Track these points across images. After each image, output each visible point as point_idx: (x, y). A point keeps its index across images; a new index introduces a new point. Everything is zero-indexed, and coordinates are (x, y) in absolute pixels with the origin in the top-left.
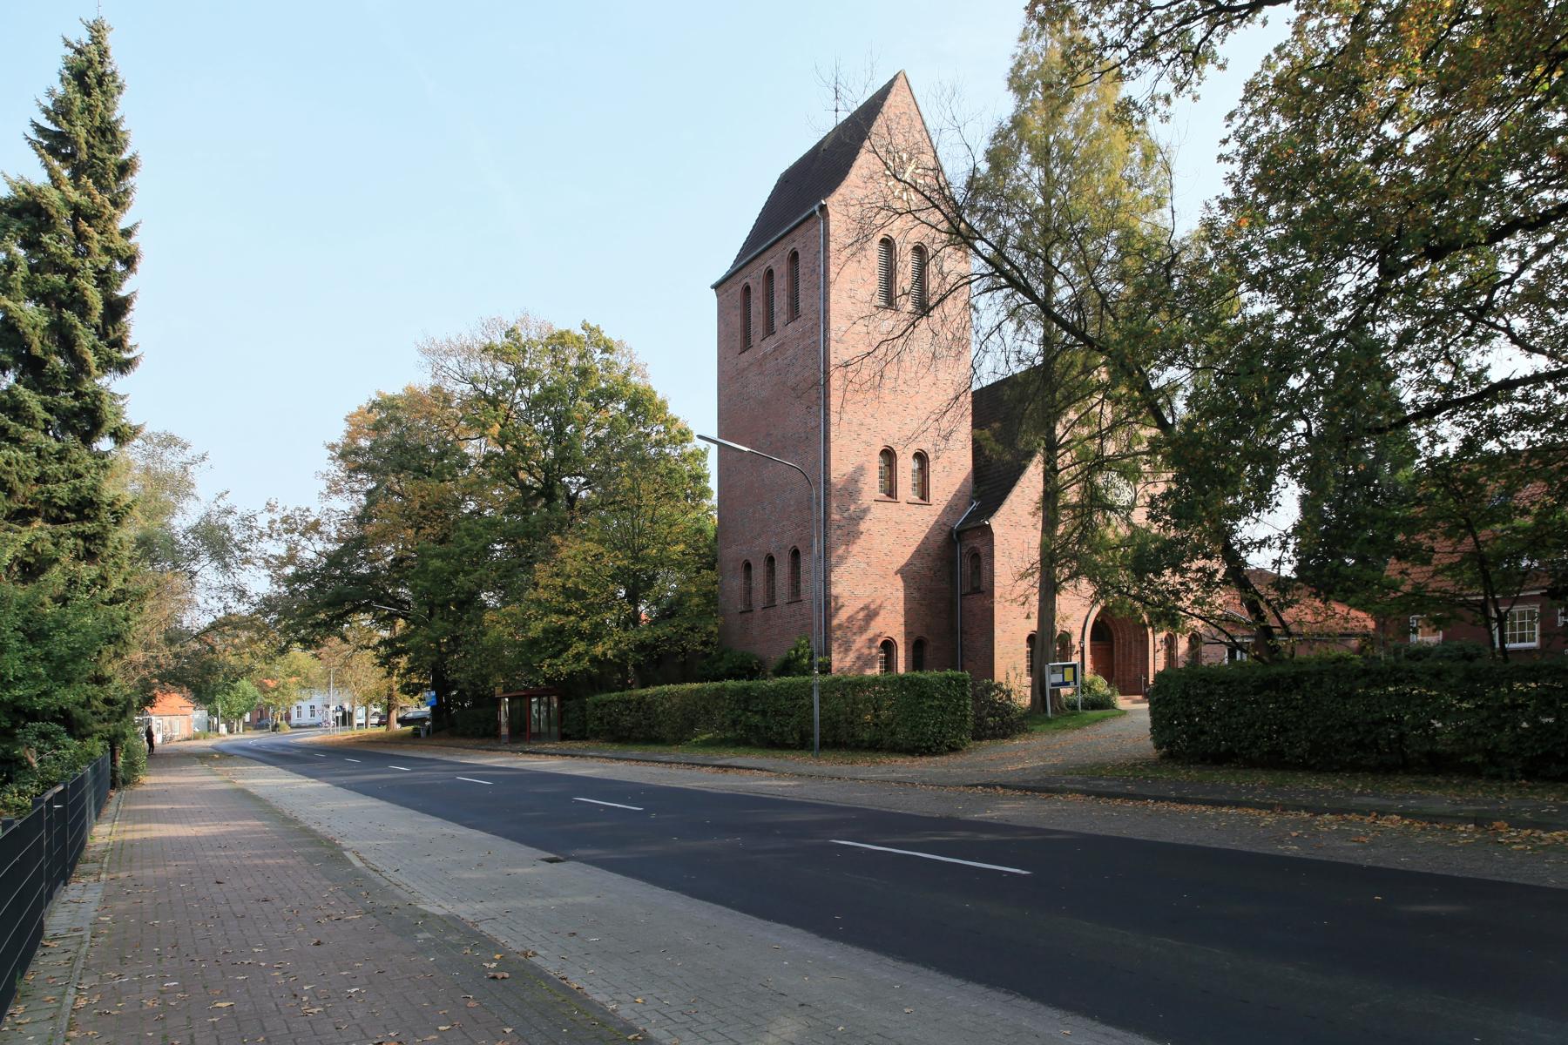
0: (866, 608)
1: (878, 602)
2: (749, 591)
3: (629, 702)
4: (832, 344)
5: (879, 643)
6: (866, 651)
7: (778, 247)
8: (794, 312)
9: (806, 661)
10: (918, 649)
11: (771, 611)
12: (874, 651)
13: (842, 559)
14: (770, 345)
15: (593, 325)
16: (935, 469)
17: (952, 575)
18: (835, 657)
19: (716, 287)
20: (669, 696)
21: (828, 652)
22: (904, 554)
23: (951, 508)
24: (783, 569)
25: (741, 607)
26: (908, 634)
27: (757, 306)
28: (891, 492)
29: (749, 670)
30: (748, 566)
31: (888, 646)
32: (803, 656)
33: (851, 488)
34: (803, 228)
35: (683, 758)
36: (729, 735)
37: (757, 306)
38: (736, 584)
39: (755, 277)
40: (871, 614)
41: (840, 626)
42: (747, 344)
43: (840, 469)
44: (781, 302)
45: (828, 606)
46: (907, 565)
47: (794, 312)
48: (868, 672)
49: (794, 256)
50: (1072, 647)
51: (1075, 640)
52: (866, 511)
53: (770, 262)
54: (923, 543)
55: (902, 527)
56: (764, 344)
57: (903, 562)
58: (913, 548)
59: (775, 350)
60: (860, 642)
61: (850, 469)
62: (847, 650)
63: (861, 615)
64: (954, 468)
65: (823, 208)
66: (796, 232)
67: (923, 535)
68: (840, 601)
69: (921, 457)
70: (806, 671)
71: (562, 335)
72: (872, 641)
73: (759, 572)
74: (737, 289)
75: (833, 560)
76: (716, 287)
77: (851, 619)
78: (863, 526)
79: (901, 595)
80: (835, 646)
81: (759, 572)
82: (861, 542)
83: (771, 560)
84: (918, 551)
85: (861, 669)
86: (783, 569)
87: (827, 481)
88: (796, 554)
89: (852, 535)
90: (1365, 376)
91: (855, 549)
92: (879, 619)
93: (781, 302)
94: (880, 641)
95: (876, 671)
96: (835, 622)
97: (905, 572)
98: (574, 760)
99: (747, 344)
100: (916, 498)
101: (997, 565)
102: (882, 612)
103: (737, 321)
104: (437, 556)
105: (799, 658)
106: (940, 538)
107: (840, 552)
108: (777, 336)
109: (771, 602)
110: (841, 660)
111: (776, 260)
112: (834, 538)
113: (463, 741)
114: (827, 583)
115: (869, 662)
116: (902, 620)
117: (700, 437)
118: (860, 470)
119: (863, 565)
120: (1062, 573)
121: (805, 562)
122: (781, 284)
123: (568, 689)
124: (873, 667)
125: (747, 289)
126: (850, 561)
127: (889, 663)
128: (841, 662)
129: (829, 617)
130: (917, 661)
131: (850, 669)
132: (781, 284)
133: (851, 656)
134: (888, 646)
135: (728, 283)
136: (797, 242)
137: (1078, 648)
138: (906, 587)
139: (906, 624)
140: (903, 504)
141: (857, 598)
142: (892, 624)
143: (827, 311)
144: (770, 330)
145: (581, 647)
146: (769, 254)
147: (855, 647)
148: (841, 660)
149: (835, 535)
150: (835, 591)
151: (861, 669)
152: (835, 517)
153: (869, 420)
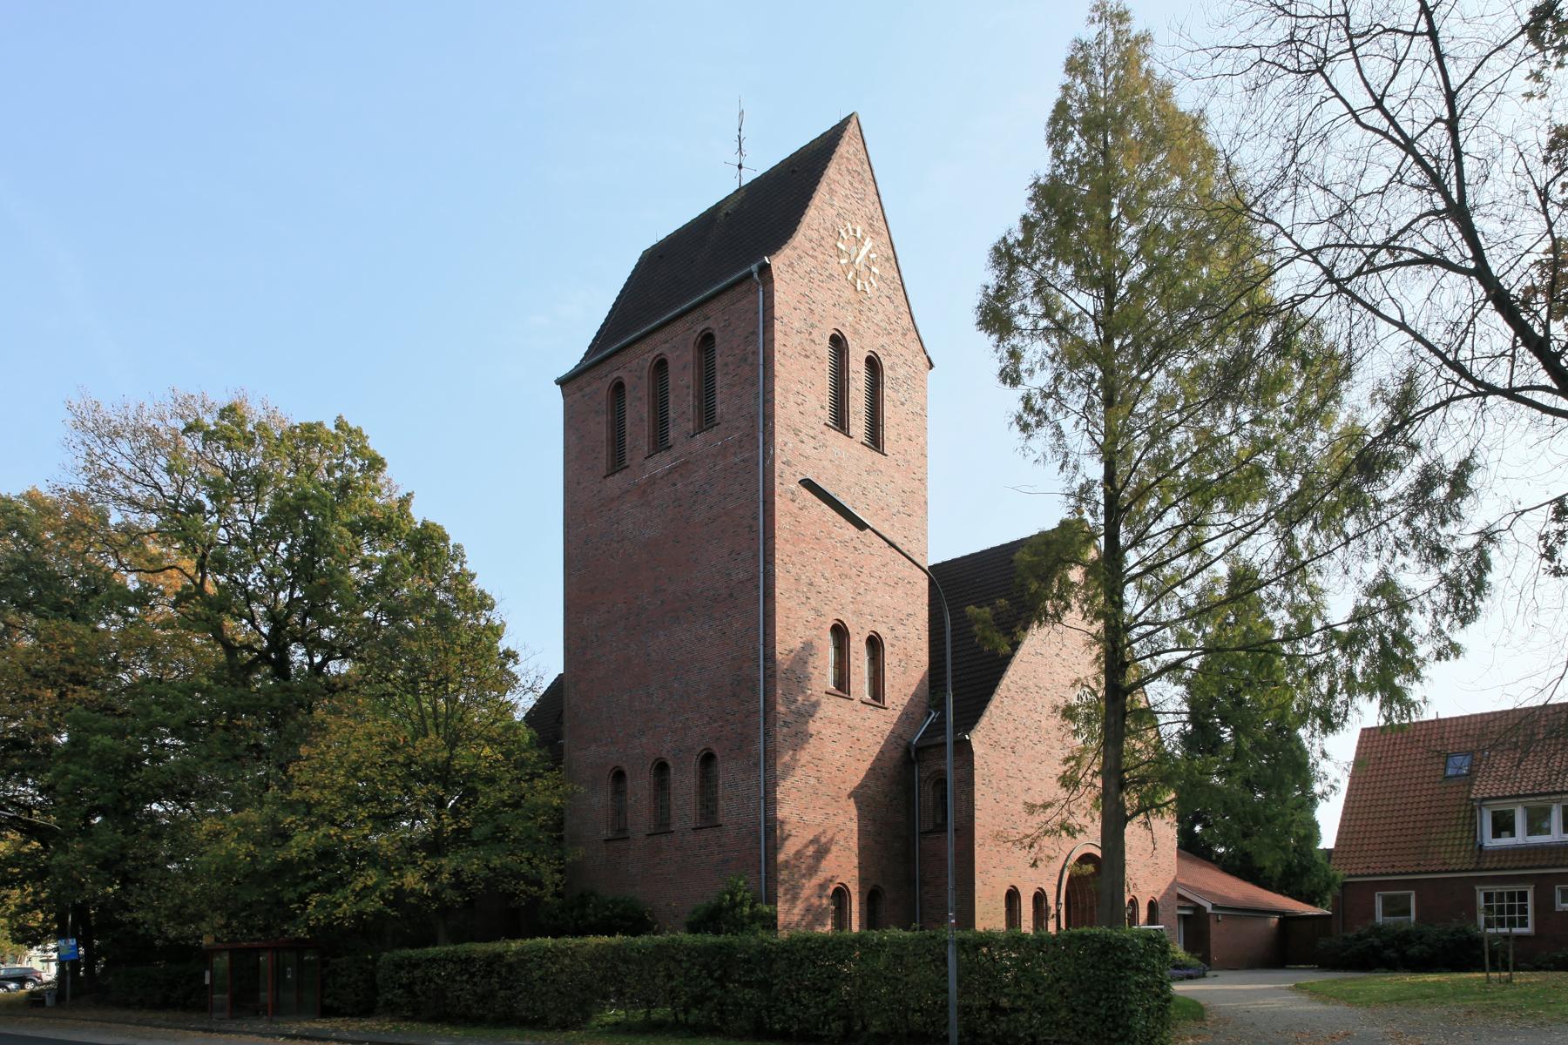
0: (815, 840)
1: (829, 835)
4: (778, 464)
5: (830, 891)
6: (815, 901)
7: (679, 326)
8: (706, 417)
9: (747, 910)
10: (872, 898)
12: (825, 902)
13: (789, 769)
14: (662, 463)
15: (353, 425)
16: (890, 658)
17: (910, 803)
18: (781, 907)
19: (563, 382)
20: (555, 955)
21: (772, 899)
22: (857, 772)
23: (907, 717)
24: (685, 782)
25: (606, 833)
26: (863, 881)
27: (638, 410)
28: (842, 683)
30: (619, 776)
31: (840, 895)
32: (742, 903)
34: (725, 299)
36: (658, 1014)
37: (638, 410)
38: (602, 798)
39: (634, 369)
40: (822, 852)
41: (787, 864)
42: (618, 462)
43: (787, 640)
44: (682, 403)
45: (771, 832)
46: (861, 786)
47: (706, 417)
48: (819, 930)
49: (707, 340)
50: (1048, 909)
51: (1051, 901)
52: (816, 705)
53: (663, 349)
55: (856, 734)
56: (650, 463)
58: (867, 765)
59: (671, 471)
60: (809, 887)
62: (795, 898)
63: (810, 850)
64: (909, 664)
65: (765, 269)
67: (877, 749)
70: (739, 926)
71: (309, 428)
72: (823, 887)
73: (640, 786)
74: (600, 387)
75: (779, 769)
76: (563, 382)
77: (799, 855)
78: (813, 727)
79: (854, 826)
80: (781, 891)
81: (640, 786)
82: (811, 748)
83: (662, 767)
85: (810, 925)
86: (685, 782)
87: (770, 657)
88: (708, 759)
91: (804, 756)
92: (831, 857)
93: (682, 403)
94: (832, 887)
95: (827, 928)
96: (781, 857)
97: (858, 795)
99: (618, 462)
100: (867, 697)
101: (977, 795)
102: (834, 848)
103: (600, 428)
104: (104, 731)
105: (735, 905)
106: (897, 754)
107: (787, 758)
109: (662, 826)
111: (678, 346)
113: (151, 1015)
114: (770, 802)
115: (819, 918)
116: (856, 861)
117: (808, 484)
118: (808, 647)
119: (813, 781)
120: (1131, 800)
121: (726, 771)
122: (682, 381)
123: (330, 941)
124: (823, 925)
126: (799, 772)
128: (789, 915)
130: (872, 918)
131: (798, 925)
132: (682, 381)
133: (799, 909)
134: (840, 895)
137: (1053, 911)
138: (861, 817)
139: (861, 867)
142: (844, 866)
143: (769, 417)
144: (660, 442)
145: (372, 877)
146: (660, 336)
147: (805, 893)
149: (782, 733)
150: (781, 813)
152: (781, 709)
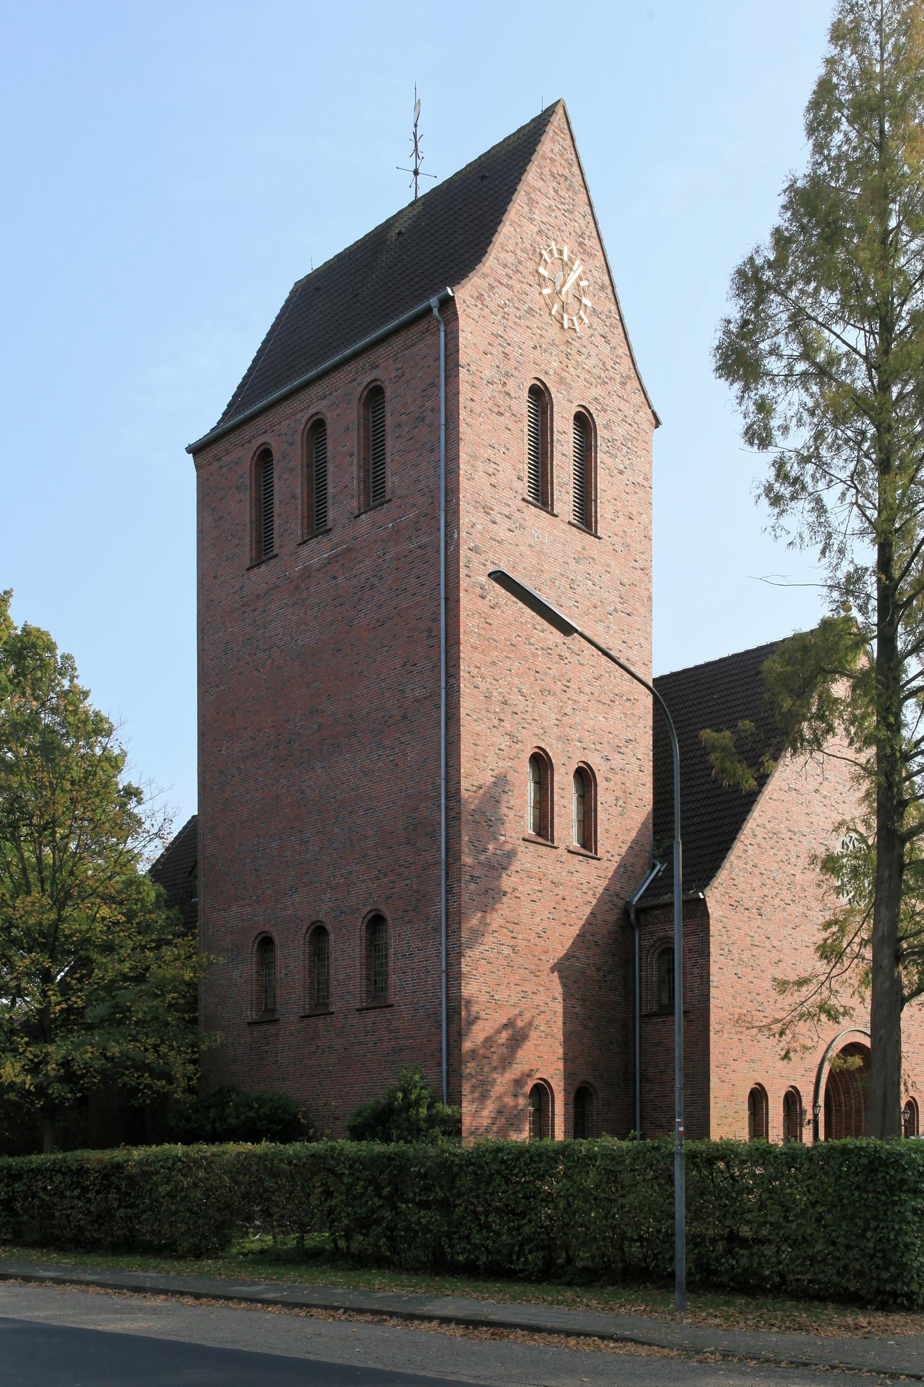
1: (527, 1016)
2: (267, 988)
3: (82, 1171)
5: (528, 1089)
6: (509, 1101)
8: (375, 492)
11: (321, 1023)
12: (522, 1101)
13: (477, 935)
14: (318, 551)
16: (604, 796)
18: (467, 1108)
19: (196, 450)
21: (455, 1099)
23: (625, 869)
24: (347, 952)
25: (250, 1014)
26: (569, 1076)
27: (289, 484)
28: (544, 828)
29: (287, 1126)
30: (266, 943)
31: (541, 1093)
32: (417, 1103)
33: (489, 819)
34: (397, 342)
35: (108, 1278)
37: (289, 484)
38: (245, 971)
39: (284, 432)
40: (518, 1039)
42: (264, 548)
43: (474, 775)
45: (455, 1014)
47: (375, 492)
49: (375, 394)
50: (803, 1112)
52: (511, 855)
54: (588, 922)
55: (561, 891)
56: (304, 551)
57: (561, 951)
58: (575, 931)
59: (329, 561)
60: (502, 1082)
61: (487, 778)
62: (484, 1097)
63: (504, 1037)
65: (448, 303)
66: (380, 351)
67: (588, 910)
68: (475, 1008)
69: (585, 777)
70: (414, 1132)
72: (518, 1083)
73: (292, 958)
74: (242, 454)
75: (465, 935)
76: (196, 450)
78: (507, 882)
79: (559, 1007)
80: (466, 1088)
81: (292, 958)
82: (505, 908)
83: (319, 932)
84: (581, 936)
85: (503, 1132)
86: (347, 952)
87: (453, 795)
88: (376, 922)
89: (492, 896)
90: (659, 840)
91: (496, 920)
92: (529, 1045)
95: (523, 1136)
96: (467, 1045)
98: (32, 1288)
99: (264, 548)
100: (575, 845)
102: (533, 1035)
103: (241, 509)
105: (409, 1105)
106: (612, 917)
107: (474, 922)
108: (335, 537)
109: (319, 1006)
110: (475, 1114)
111: (337, 402)
112: (465, 897)
114: (454, 977)
115: (513, 1121)
118: (501, 782)
119: (507, 951)
121: (398, 938)
124: (520, 1130)
125: (265, 456)
126: (489, 939)
127: (541, 1125)
128: (478, 1118)
129: (456, 1035)
130: (580, 1125)
134: (541, 1093)
135: (224, 444)
136: (384, 367)
137: (809, 1116)
138: (567, 996)
140: (562, 851)
141: (499, 1006)
142: (546, 1057)
144: (316, 524)
146: (316, 390)
148: (475, 1114)
149: (468, 890)
150: (469, 989)
151: (503, 1132)
152: (467, 860)
153: (515, 698)
